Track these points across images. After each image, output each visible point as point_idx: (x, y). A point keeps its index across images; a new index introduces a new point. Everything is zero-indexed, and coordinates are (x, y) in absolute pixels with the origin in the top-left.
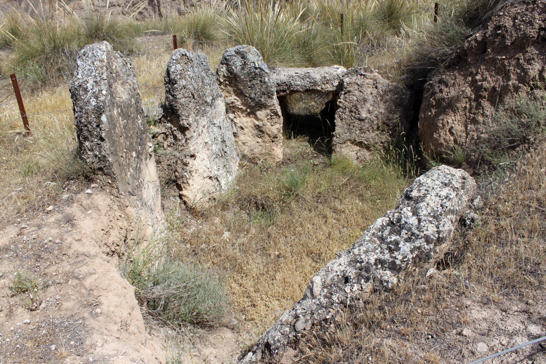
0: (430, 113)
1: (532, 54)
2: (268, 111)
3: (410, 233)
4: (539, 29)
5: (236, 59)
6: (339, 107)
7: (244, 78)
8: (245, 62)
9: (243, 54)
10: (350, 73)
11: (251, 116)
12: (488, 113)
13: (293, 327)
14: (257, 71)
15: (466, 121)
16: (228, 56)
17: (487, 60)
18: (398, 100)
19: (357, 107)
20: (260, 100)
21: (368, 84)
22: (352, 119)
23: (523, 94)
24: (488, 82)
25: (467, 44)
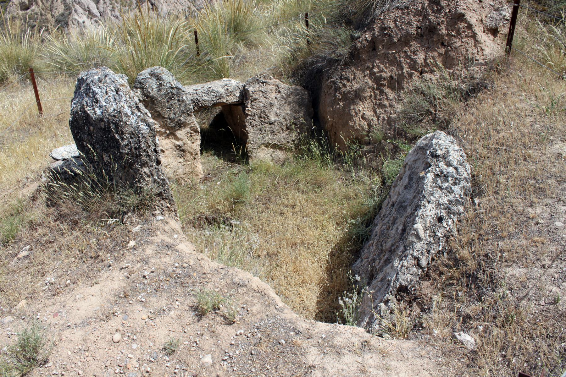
0: (338, 106)
1: (416, 47)
2: (188, 129)
3: (454, 179)
4: (416, 28)
5: (150, 81)
6: (247, 115)
7: (162, 100)
8: (160, 84)
9: (158, 76)
10: (252, 83)
11: (170, 137)
12: (391, 97)
13: (419, 265)
14: (173, 91)
15: (374, 107)
16: (142, 79)
17: (380, 55)
18: (300, 100)
19: (265, 113)
20: (180, 120)
21: (271, 90)
22: (262, 124)
23: (415, 78)
24: (386, 73)
25: (359, 45)
